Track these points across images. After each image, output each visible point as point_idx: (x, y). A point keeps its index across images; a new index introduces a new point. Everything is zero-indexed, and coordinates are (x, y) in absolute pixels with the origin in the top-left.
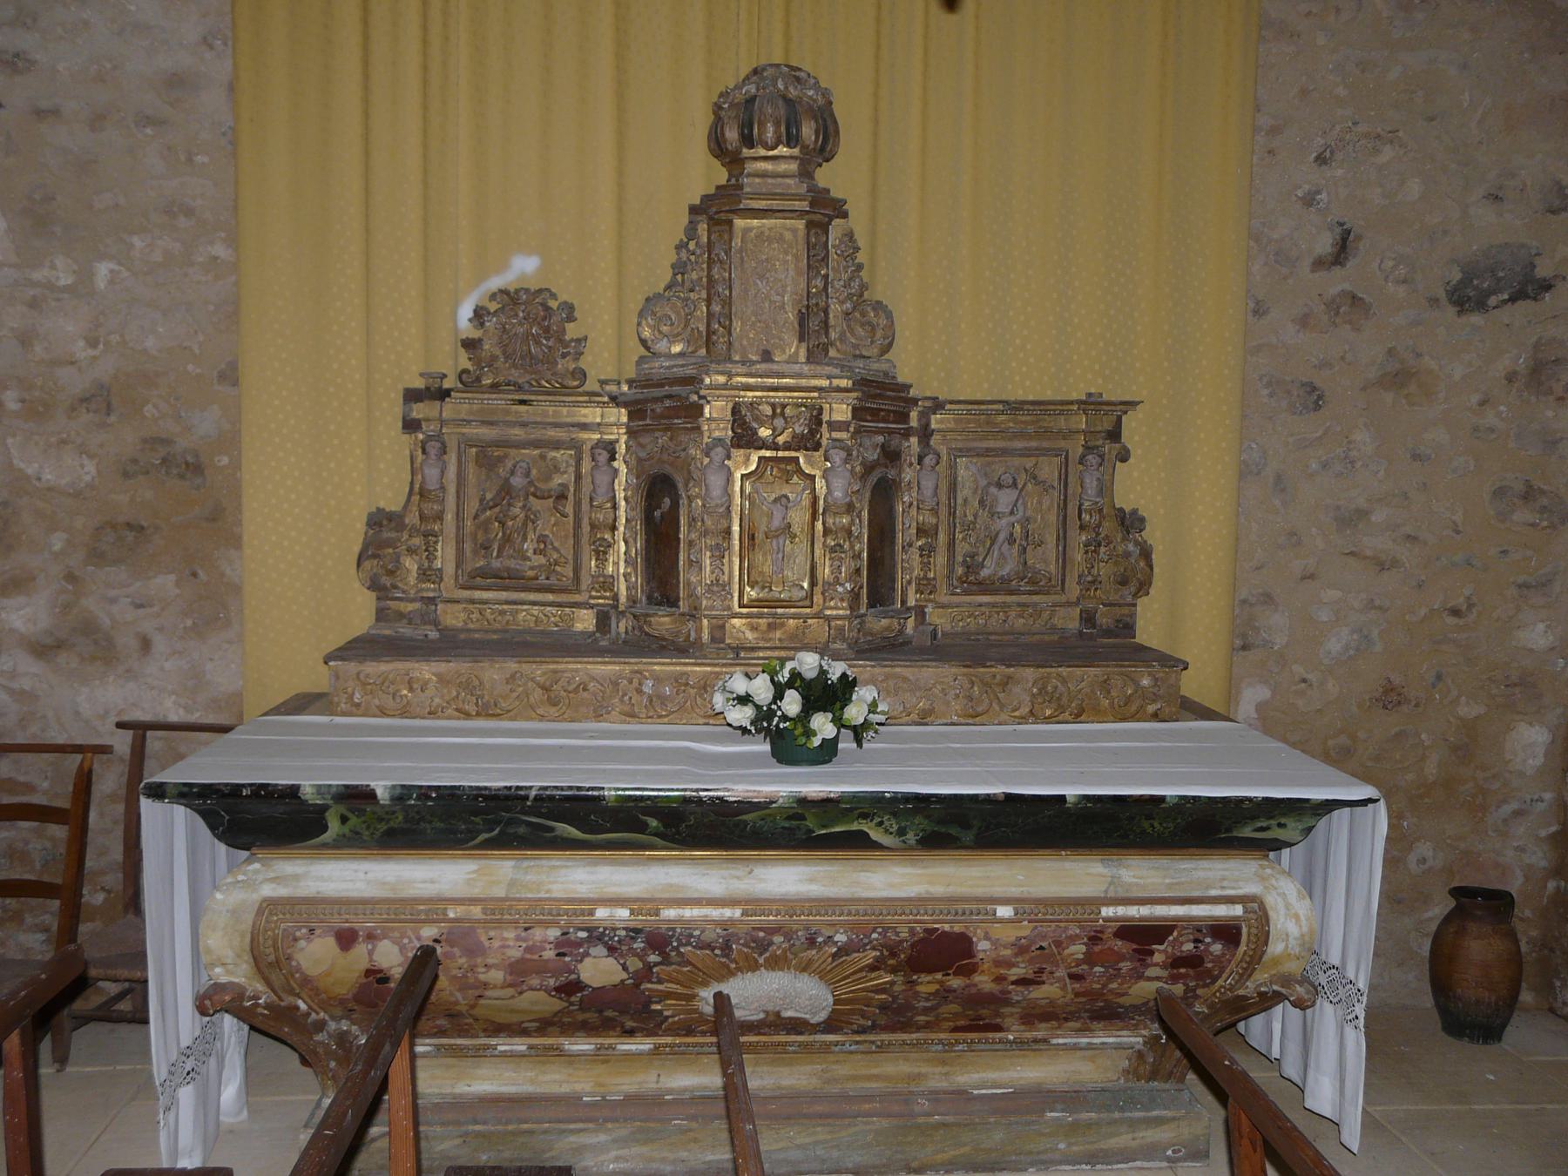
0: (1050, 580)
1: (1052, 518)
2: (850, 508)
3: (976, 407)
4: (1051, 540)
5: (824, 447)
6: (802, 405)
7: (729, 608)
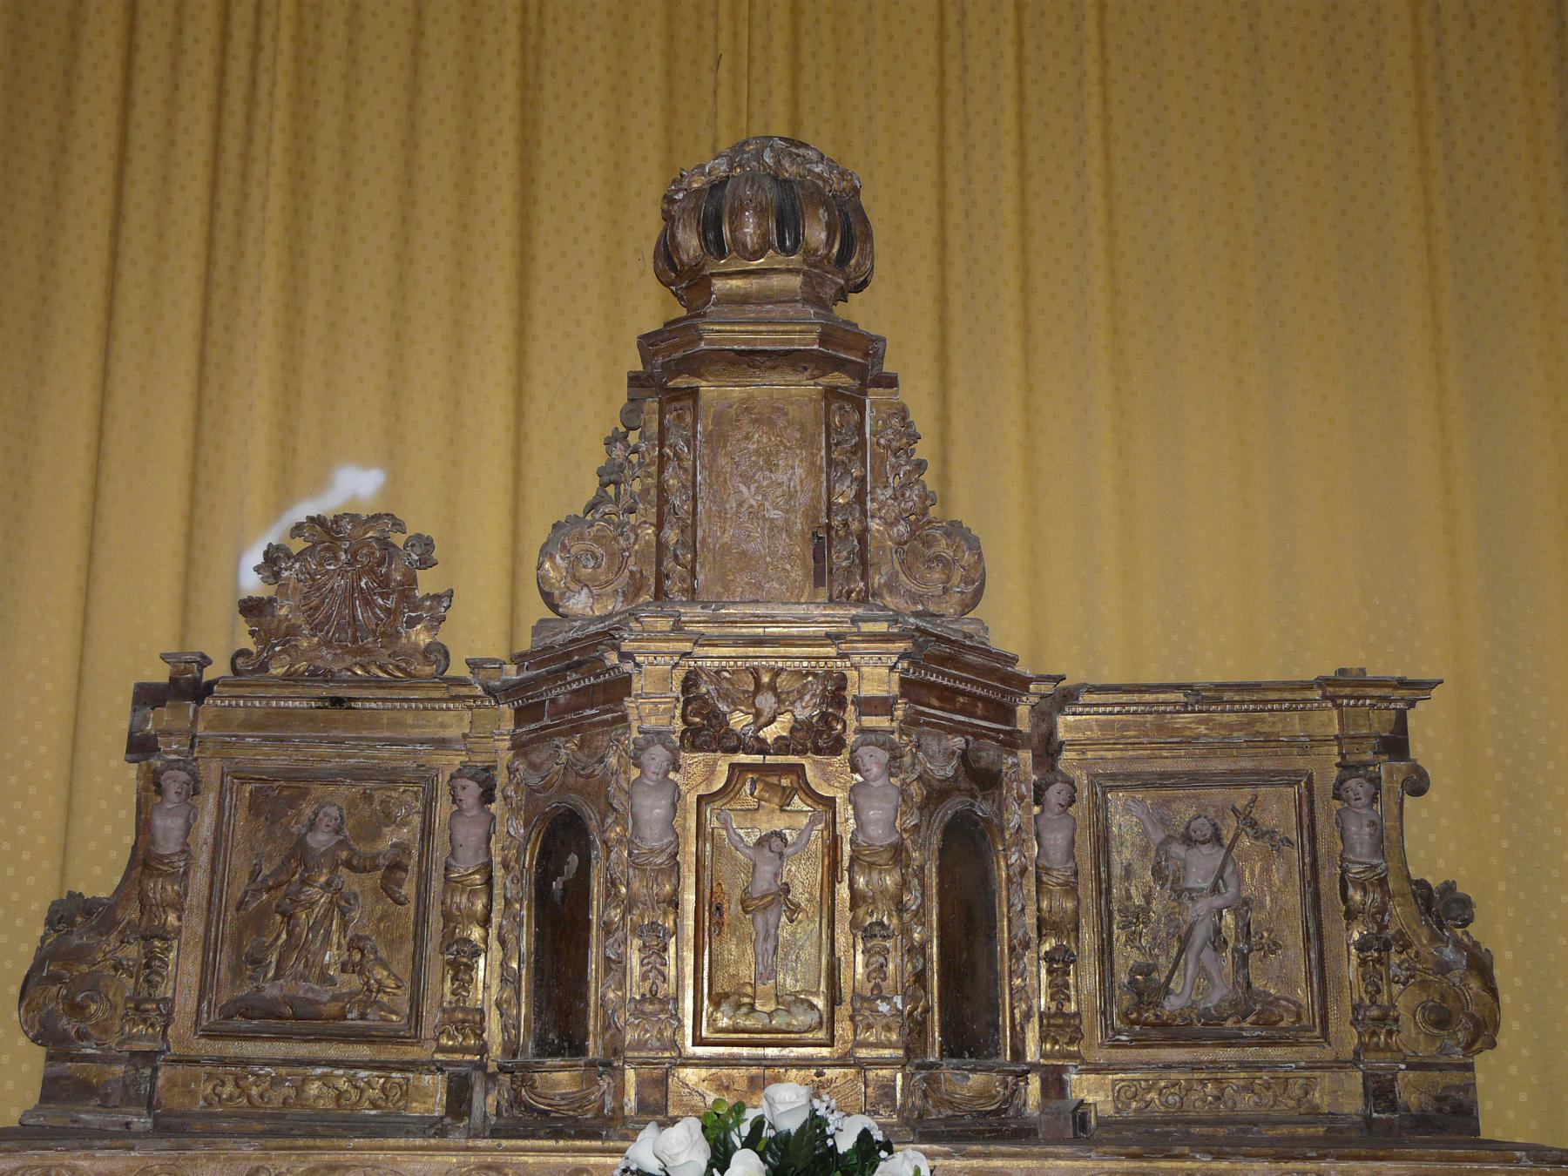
0: (1299, 1016)
1: (1293, 899)
2: (898, 853)
3: (1135, 697)
4: (1293, 938)
6: (808, 674)
7: (674, 1045)
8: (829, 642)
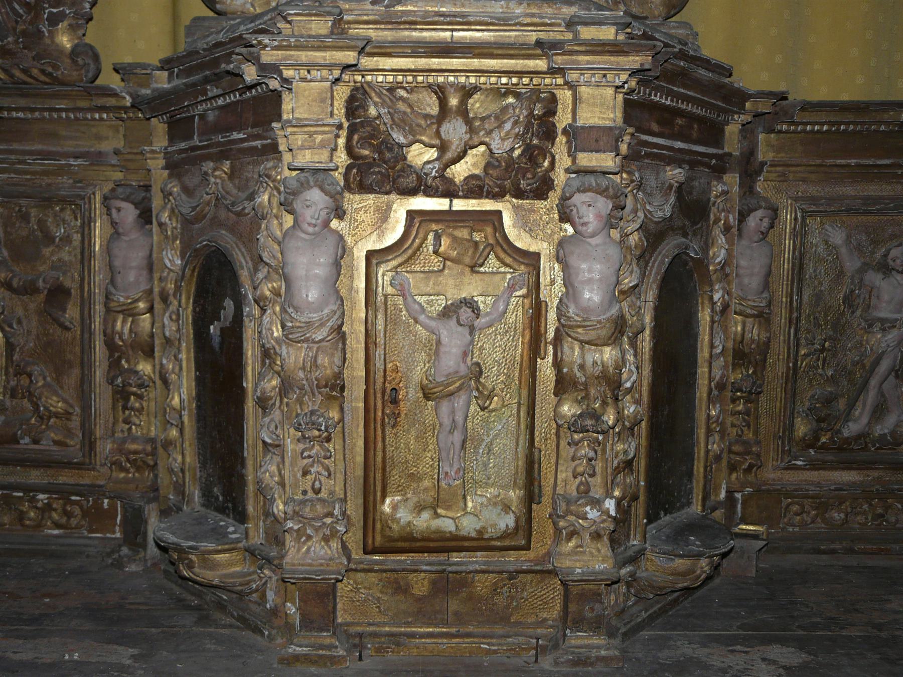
5: (559, 190)
8: (539, 51)
